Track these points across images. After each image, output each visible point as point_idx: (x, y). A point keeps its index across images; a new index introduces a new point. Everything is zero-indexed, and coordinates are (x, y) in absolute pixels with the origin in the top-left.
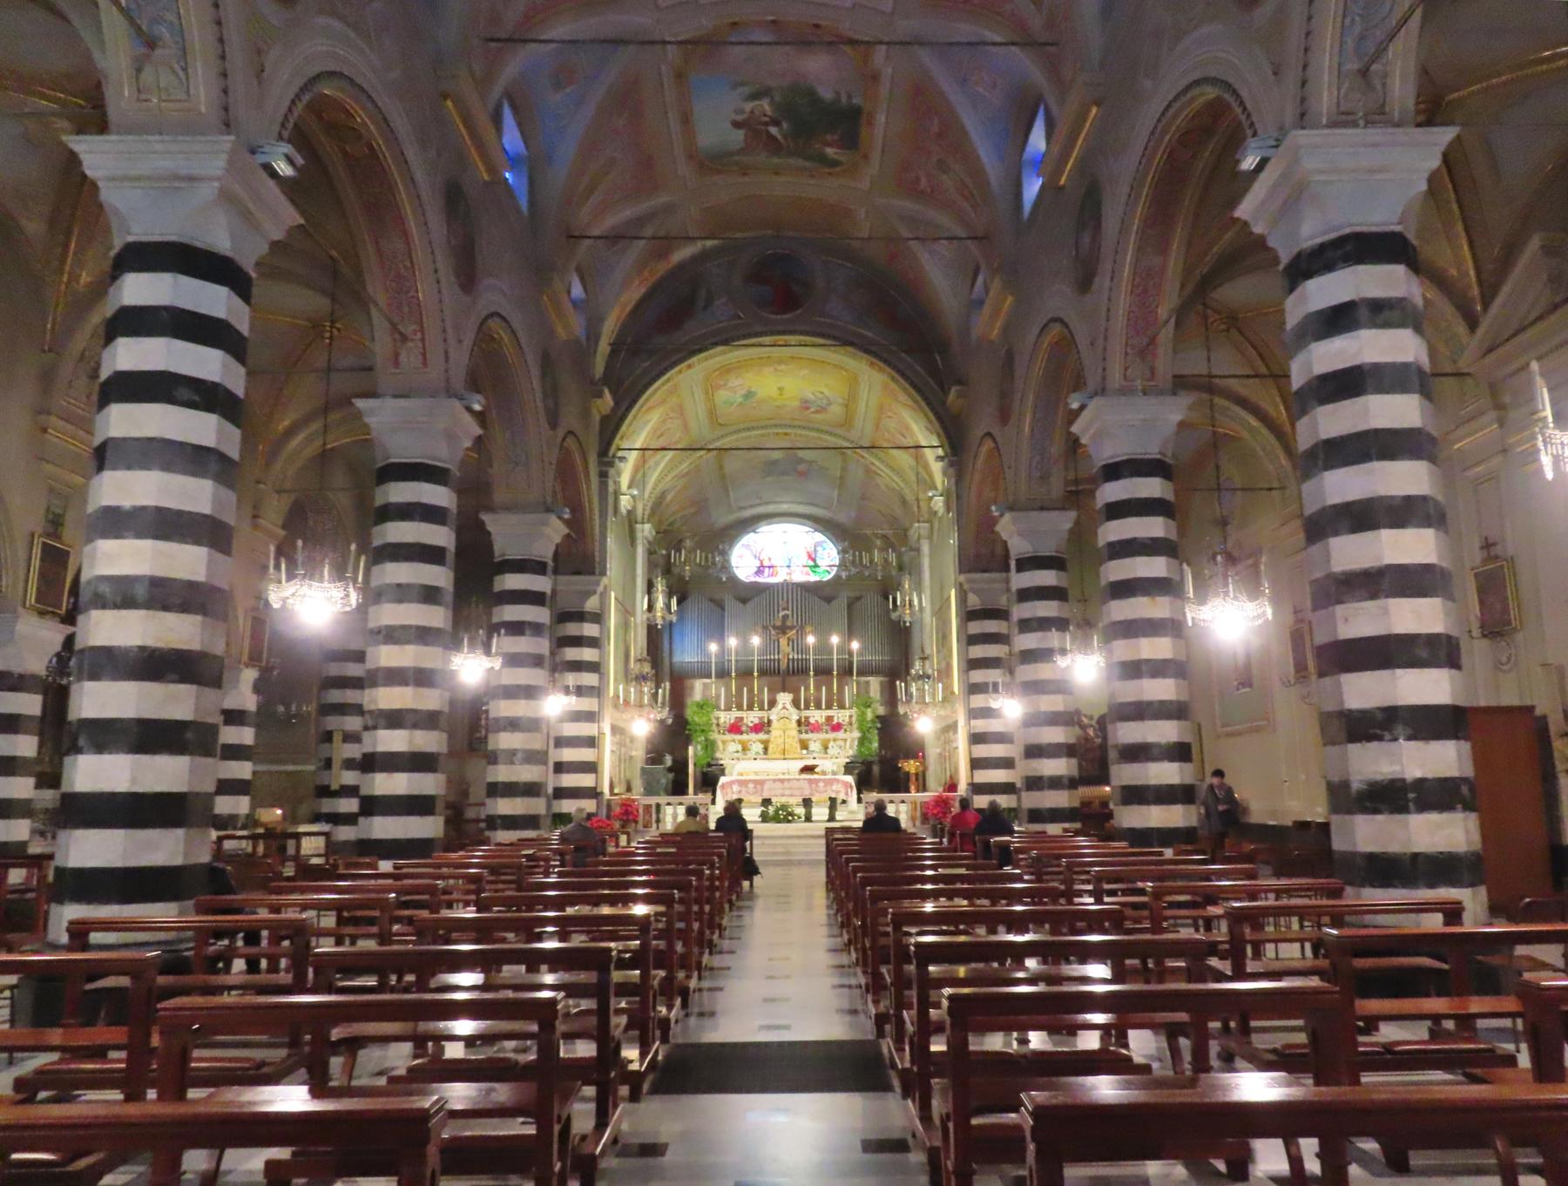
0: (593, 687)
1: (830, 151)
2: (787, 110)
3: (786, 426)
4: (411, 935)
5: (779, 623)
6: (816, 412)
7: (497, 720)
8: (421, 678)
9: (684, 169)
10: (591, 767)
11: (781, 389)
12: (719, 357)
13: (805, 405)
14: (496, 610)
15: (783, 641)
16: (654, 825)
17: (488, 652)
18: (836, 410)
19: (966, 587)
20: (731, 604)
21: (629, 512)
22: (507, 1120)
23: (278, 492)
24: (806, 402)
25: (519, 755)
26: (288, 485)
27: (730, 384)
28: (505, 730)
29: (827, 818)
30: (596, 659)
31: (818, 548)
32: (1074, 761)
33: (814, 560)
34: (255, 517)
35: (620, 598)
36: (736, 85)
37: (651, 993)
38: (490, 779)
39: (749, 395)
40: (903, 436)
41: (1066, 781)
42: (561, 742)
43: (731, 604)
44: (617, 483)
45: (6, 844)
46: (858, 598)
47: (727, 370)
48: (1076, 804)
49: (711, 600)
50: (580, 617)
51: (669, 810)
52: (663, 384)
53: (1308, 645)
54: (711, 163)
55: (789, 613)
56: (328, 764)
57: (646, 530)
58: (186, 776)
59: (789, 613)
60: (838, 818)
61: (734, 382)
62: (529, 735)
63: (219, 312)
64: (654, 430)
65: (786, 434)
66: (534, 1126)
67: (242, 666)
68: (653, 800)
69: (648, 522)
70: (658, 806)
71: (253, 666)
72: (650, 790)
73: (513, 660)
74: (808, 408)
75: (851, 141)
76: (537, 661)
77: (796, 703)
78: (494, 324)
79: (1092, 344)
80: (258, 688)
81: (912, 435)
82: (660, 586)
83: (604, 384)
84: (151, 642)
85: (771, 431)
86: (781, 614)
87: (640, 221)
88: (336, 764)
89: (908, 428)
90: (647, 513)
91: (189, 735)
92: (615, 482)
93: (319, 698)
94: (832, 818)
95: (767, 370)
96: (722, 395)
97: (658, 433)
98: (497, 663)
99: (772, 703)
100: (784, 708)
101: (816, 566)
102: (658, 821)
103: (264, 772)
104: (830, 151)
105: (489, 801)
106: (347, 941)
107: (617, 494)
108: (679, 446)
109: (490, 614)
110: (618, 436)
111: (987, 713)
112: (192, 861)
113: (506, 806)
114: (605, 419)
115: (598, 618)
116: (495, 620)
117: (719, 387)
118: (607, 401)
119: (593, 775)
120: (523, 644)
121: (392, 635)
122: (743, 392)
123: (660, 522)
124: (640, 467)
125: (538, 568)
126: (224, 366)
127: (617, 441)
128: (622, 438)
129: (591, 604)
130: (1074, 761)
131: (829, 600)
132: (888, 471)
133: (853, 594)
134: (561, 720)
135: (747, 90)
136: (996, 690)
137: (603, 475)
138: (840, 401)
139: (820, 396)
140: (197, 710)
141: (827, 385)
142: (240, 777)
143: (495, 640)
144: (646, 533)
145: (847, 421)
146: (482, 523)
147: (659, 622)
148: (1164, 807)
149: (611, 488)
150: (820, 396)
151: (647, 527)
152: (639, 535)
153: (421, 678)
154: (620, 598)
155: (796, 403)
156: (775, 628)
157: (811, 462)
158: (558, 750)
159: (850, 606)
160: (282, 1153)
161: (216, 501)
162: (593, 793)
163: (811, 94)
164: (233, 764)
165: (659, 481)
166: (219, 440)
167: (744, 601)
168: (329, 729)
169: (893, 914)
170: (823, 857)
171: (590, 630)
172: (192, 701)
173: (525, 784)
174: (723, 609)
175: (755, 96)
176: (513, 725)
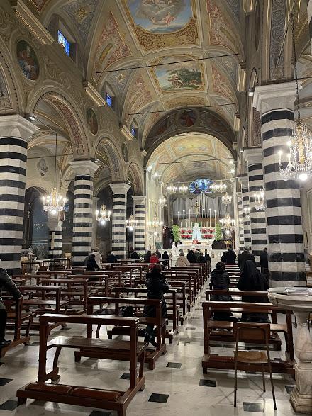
1: (195, 84)
2: (181, 76)
4: (234, 312)
8: (122, 226)
9: (158, 93)
10: (144, 243)
12: (173, 139)
36: (167, 72)
54: (165, 91)
56: (50, 240)
66: (38, 337)
75: (200, 82)
77: (200, 226)
80: (63, 226)
87: (150, 107)
88: (53, 241)
99: (194, 226)
104: (195, 84)
106: (57, 284)
114: (145, 157)
121: (117, 218)
125: (87, 178)
129: (142, 203)
135: (170, 72)
148: (285, 244)
153: (122, 226)
160: (78, 350)
162: (144, 249)
163: (186, 70)
171: (142, 209)
175: (172, 74)
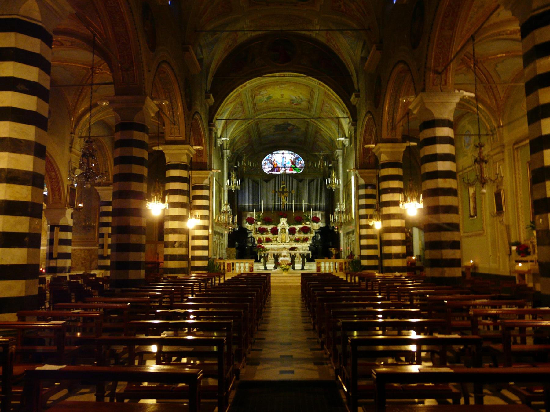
0: (207, 216)
3: (284, 110)
5: (281, 190)
6: (296, 105)
7: (167, 229)
11: (282, 95)
13: (292, 102)
14: (167, 185)
15: (283, 197)
16: (232, 271)
17: (163, 201)
18: (304, 104)
19: (358, 175)
20: (262, 184)
21: (221, 145)
22: (203, 265)
23: (79, 137)
24: (292, 100)
25: (177, 244)
26: (84, 135)
27: (262, 93)
28: (171, 233)
29: (301, 268)
30: (208, 205)
31: (297, 160)
32: (405, 247)
33: (295, 165)
34: (71, 148)
35: (218, 180)
37: (232, 356)
38: (165, 253)
39: (269, 98)
40: (332, 114)
41: (401, 255)
42: (194, 238)
43: (262, 184)
44: (216, 134)
45: (2, 266)
46: (312, 180)
47: (261, 87)
48: (405, 265)
49: (253, 181)
50: (201, 187)
51: (238, 265)
52: (235, 93)
53: (460, 198)
55: (285, 186)
57: (227, 153)
58: (26, 258)
59: (285, 186)
60: (305, 268)
61: (263, 92)
62: (179, 235)
63: (37, 51)
64: (231, 112)
65: (284, 114)
67: (67, 208)
68: (231, 261)
69: (228, 149)
70: (233, 264)
71: (71, 208)
72: (229, 258)
73: (173, 205)
74: (293, 103)
76: (182, 205)
78: (164, 65)
79: (419, 70)
81: (336, 113)
82: (233, 174)
83: (210, 93)
84: (8, 198)
85: (278, 112)
86: (282, 187)
89: (334, 111)
90: (228, 146)
91: (27, 239)
92: (215, 133)
93: (99, 221)
94: (303, 269)
95: (277, 87)
96: (258, 97)
97: (233, 114)
98: (166, 205)
100: (283, 224)
101: (296, 167)
102: (233, 269)
103: (78, 249)
105: (165, 262)
107: (216, 138)
108: (241, 118)
109: (164, 187)
110: (216, 114)
111: (368, 227)
112: (29, 294)
113: (172, 264)
114: (211, 107)
115: (208, 188)
116: (167, 188)
117: (256, 95)
118: (212, 99)
119: (207, 251)
120: (177, 199)
122: (267, 97)
123: (233, 150)
124: (225, 128)
126: (40, 75)
127: (216, 116)
128: (218, 115)
130: (405, 247)
131: (301, 181)
132: (325, 129)
133: (311, 178)
134: (194, 229)
136: (372, 217)
137: (210, 130)
138: (306, 100)
139: (298, 98)
140: (30, 227)
141: (301, 93)
142: (68, 252)
143: (167, 197)
144: (228, 154)
145: (309, 108)
146: (51, 86)
147: (233, 189)
149: (214, 135)
150: (299, 98)
151: (228, 151)
152: (225, 155)
154: (218, 180)
155: (288, 101)
156: (279, 192)
157: (294, 126)
158: (193, 241)
159: (309, 183)
161: (36, 135)
164: (64, 247)
165: (232, 133)
166: (37, 108)
167: (267, 181)
168: (103, 232)
169: (333, 311)
170: (300, 284)
172: (27, 224)
173: (179, 255)
174: (258, 185)
176: (174, 231)
